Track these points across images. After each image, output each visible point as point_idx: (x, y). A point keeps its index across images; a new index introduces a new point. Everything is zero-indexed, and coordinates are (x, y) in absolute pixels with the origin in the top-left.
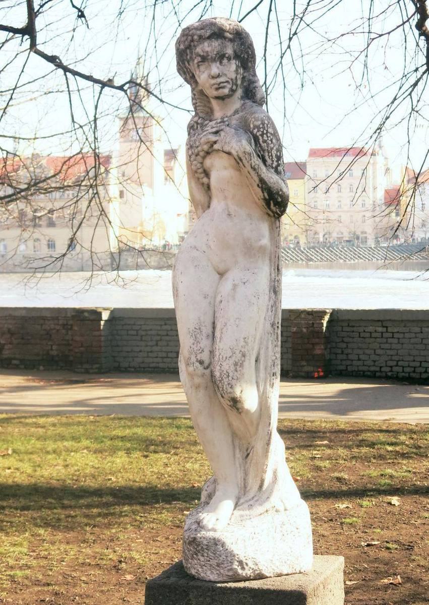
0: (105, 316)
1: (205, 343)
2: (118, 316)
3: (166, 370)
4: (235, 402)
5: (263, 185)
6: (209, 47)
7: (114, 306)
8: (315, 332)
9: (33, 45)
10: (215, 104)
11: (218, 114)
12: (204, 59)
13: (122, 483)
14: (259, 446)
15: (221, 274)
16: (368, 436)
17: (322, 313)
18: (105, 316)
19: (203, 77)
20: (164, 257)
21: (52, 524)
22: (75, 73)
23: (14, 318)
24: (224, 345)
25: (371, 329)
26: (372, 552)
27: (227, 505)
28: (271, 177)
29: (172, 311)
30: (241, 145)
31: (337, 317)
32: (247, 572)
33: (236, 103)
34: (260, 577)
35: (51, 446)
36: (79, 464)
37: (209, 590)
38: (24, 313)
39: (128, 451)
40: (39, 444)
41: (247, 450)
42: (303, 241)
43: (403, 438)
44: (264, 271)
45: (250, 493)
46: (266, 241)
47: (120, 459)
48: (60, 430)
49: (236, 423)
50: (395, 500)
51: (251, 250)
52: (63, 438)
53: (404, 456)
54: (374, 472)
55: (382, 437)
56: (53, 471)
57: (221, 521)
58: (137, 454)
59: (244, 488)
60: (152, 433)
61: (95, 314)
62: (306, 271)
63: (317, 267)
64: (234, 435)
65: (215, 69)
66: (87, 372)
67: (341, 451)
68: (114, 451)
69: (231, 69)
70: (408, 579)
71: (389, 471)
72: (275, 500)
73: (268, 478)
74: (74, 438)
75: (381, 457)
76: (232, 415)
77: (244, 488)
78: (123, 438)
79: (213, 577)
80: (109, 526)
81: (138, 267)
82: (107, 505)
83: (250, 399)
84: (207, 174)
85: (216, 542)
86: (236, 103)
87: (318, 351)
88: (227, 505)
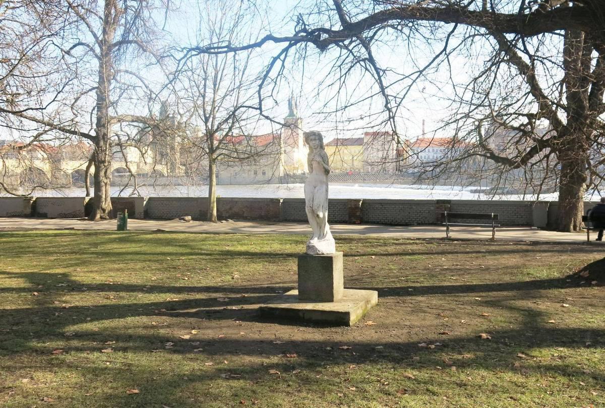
0: (281, 201)
1: (311, 202)
2: (286, 201)
3: (305, 221)
4: (318, 216)
5: (324, 168)
6: (313, 137)
7: (284, 198)
8: (357, 207)
9: (261, 113)
10: (314, 150)
11: (314, 152)
12: (311, 140)
13: (289, 252)
14: (323, 225)
15: (315, 187)
16: (370, 240)
17: (360, 200)
18: (281, 201)
19: (311, 144)
20: (302, 179)
21: (270, 262)
22: (274, 122)
23: (248, 201)
24: (315, 203)
25: (377, 206)
26: (363, 268)
27: (316, 239)
28: (326, 166)
29: (304, 199)
30: (319, 159)
31: (365, 201)
32: (320, 253)
33: (318, 149)
34: (323, 254)
35: (266, 242)
36: (276, 247)
37: (312, 257)
38: (252, 200)
39: (291, 244)
40: (261, 242)
41: (321, 227)
42: (362, 171)
43: (381, 241)
44: (325, 186)
45: (321, 236)
46: (325, 180)
47: (288, 246)
48: (269, 238)
49: (318, 221)
50: (373, 257)
51: (321, 182)
52: (269, 240)
53: (380, 246)
54: (369, 250)
55: (374, 241)
56: (267, 249)
57: (315, 242)
58: (293, 245)
59: (320, 235)
60: (299, 239)
61: (278, 200)
62: (363, 184)
63: (368, 183)
64: (318, 223)
65: (314, 142)
66: (275, 221)
67: (360, 244)
68: (286, 244)
69: (317, 142)
70: (372, 274)
71: (374, 249)
72: (326, 238)
73: (325, 233)
74: (273, 240)
75: (372, 246)
76: (317, 218)
77: (320, 235)
78: (289, 240)
79: (312, 254)
80: (286, 262)
81: (294, 183)
82: (285, 257)
83: (321, 215)
84: (312, 165)
85: (313, 246)
86: (318, 149)
87: (358, 214)
88: (316, 239)
